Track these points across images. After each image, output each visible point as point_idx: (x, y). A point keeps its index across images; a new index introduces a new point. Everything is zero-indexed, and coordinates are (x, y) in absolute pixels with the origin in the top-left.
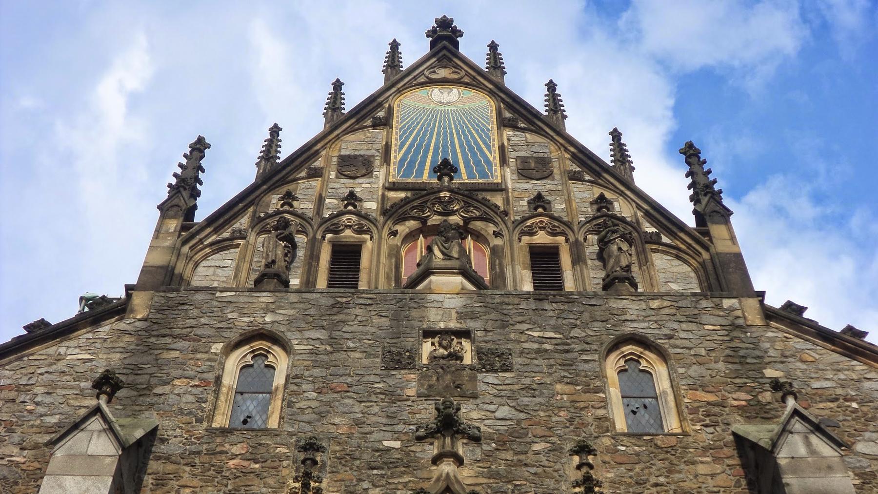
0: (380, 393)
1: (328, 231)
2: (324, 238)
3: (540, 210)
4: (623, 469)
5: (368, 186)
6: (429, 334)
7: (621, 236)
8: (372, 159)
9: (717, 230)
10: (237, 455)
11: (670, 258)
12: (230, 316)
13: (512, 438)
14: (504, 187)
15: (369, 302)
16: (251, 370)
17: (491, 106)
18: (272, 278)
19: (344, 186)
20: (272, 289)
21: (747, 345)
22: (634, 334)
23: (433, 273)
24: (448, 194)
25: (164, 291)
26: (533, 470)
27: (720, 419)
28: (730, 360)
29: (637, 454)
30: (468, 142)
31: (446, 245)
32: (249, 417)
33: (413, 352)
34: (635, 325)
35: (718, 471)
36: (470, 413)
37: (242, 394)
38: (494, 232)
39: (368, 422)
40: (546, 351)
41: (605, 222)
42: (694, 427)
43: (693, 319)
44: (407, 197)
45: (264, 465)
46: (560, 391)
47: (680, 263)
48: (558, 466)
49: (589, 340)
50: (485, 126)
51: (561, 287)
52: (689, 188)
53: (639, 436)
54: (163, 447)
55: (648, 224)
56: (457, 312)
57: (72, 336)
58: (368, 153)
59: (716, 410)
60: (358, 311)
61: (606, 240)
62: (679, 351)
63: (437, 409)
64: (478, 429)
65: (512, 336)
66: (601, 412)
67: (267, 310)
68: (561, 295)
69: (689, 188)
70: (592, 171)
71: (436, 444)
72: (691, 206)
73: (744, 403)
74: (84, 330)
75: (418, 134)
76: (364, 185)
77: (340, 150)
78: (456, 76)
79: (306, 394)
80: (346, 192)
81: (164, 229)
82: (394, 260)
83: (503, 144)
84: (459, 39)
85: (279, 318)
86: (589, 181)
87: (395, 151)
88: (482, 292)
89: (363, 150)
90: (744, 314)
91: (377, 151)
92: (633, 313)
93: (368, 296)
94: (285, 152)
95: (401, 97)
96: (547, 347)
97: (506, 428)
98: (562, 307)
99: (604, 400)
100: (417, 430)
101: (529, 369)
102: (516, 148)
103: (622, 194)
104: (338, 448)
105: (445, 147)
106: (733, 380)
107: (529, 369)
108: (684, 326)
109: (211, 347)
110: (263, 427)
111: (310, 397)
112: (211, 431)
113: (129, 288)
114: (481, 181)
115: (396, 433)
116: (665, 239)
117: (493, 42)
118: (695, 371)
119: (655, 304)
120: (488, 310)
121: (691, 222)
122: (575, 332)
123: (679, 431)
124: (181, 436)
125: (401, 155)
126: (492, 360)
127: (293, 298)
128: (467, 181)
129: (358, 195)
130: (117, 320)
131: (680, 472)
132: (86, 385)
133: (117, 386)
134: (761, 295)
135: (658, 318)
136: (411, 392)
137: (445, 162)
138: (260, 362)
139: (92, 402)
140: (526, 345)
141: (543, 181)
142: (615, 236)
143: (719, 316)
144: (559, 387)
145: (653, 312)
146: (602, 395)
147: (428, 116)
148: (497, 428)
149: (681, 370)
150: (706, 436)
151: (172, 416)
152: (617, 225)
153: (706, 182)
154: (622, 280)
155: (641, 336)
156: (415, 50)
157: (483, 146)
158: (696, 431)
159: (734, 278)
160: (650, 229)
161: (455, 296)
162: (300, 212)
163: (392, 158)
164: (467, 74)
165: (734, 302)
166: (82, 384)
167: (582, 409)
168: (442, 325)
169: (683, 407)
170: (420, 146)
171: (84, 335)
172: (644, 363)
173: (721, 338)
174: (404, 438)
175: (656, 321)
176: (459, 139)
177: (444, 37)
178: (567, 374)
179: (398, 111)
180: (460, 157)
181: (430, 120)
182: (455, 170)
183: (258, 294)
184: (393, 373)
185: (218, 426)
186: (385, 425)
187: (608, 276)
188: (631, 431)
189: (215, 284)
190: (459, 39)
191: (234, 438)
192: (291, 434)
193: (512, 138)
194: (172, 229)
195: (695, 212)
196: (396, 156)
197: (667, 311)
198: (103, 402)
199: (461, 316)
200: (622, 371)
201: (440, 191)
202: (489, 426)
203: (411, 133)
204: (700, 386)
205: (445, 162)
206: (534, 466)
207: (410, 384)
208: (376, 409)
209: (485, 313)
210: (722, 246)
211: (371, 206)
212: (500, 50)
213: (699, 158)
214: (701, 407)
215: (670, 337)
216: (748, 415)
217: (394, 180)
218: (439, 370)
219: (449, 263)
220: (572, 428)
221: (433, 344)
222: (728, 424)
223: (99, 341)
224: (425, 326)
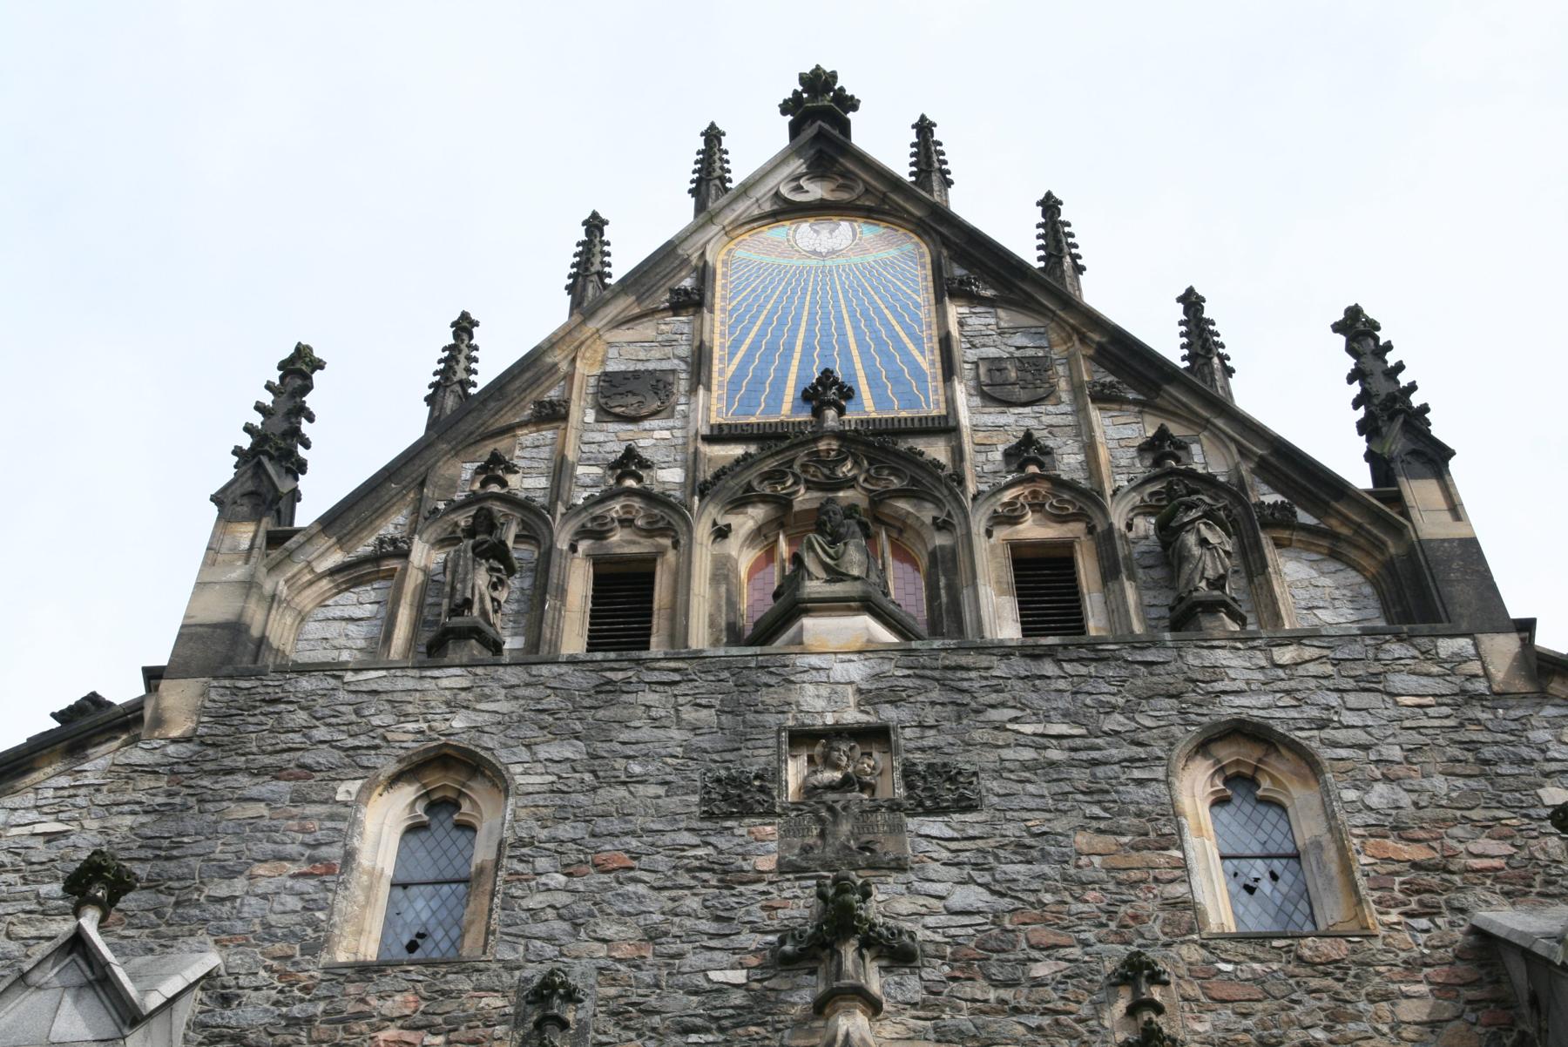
0: (702, 869)
1: (583, 533)
2: (573, 548)
3: (1033, 469)
4: (1227, 1013)
5: (666, 434)
6: (802, 738)
7: (1206, 515)
8: (671, 378)
9: (1420, 493)
10: (392, 1020)
11: (1316, 557)
12: (376, 721)
13: (981, 956)
14: (952, 423)
15: (677, 677)
16: (423, 835)
17: (922, 256)
18: (448, 634)
19: (614, 439)
20: (465, 660)
21: (1500, 737)
22: (1242, 722)
23: (807, 612)
24: (835, 445)
25: (231, 677)
26: (1034, 1021)
27: (1441, 899)
28: (1459, 768)
29: (1257, 980)
30: (874, 331)
31: (831, 551)
32: (421, 936)
33: (769, 775)
34: (1238, 701)
35: (1446, 1015)
36: (887, 902)
37: (405, 886)
38: (935, 519)
39: (675, 930)
40: (1052, 764)
41: (1172, 487)
42: (1386, 918)
43: (1371, 684)
44: (747, 455)
45: (452, 1036)
46: (1085, 848)
47: (1339, 566)
48: (1085, 1010)
49: (1142, 736)
50: (910, 298)
51: (1081, 629)
52: (1356, 404)
53: (1262, 938)
54: (228, 1013)
55: (1264, 488)
56: (859, 691)
57: (20, 784)
58: (666, 365)
59: (1433, 879)
60: (650, 698)
61: (1173, 524)
62: (1343, 753)
63: (821, 895)
64: (912, 935)
65: (977, 735)
66: (1178, 890)
67: (453, 706)
68: (1080, 646)
69: (1356, 404)
70: (1139, 381)
71: (821, 972)
72: (1361, 444)
73: (1496, 863)
74: (49, 770)
75: (767, 322)
76: (657, 434)
77: (603, 362)
78: (844, 196)
79: (543, 879)
80: (620, 449)
81: (228, 542)
82: (723, 589)
83: (948, 334)
84: (851, 115)
85: (480, 719)
86: (1135, 402)
87: (721, 359)
88: (914, 644)
89: (654, 362)
90: (1485, 669)
91: (682, 359)
92: (1238, 675)
93: (672, 665)
94: (486, 373)
95: (731, 246)
96: (1055, 754)
97: (971, 931)
98: (1083, 670)
99: (1183, 865)
100: (782, 942)
101: (1015, 803)
102: (976, 341)
103: (1205, 425)
104: (612, 991)
105: (826, 345)
106: (1466, 813)
107: (1015, 803)
108: (1352, 700)
109: (335, 791)
110: (451, 954)
111: (552, 884)
112: (336, 973)
113: (153, 676)
114: (903, 414)
115: (734, 951)
116: (1304, 517)
117: (923, 118)
118: (1379, 795)
119: (1285, 655)
120: (926, 683)
121: (1360, 477)
122: (1115, 722)
123: (1353, 926)
124: (270, 987)
125: (733, 367)
126: (941, 789)
127: (511, 675)
128: (874, 415)
129: (645, 455)
130: (126, 744)
131: (1357, 1018)
132: (56, 888)
133: (121, 885)
134: (1526, 627)
135: (1293, 684)
136: (766, 863)
137: (827, 376)
138: (443, 816)
139: (62, 928)
140: (1008, 754)
141: (1036, 408)
142: (1193, 514)
143: (1428, 675)
144: (1082, 840)
145: (1281, 673)
146: (1177, 854)
147: (789, 283)
148: (952, 931)
149: (1350, 795)
150: (1415, 938)
151: (248, 944)
152: (1197, 492)
153: (1392, 389)
154: (1212, 607)
155: (1258, 725)
156: (759, 141)
157: (906, 340)
158: (1390, 926)
159: (1460, 593)
160: (1272, 498)
161: (855, 657)
162: (522, 495)
163: (715, 375)
164: (868, 191)
165: (1464, 644)
166: (44, 889)
167: (1133, 885)
168: (830, 720)
169: (1358, 875)
170: (772, 348)
171: (50, 778)
172: (1266, 783)
173: (1437, 723)
174: (754, 961)
175: (1288, 692)
176: (856, 328)
177: (819, 110)
178: (1097, 810)
179: (724, 275)
180: (858, 366)
181: (794, 292)
182: (847, 393)
183: (436, 673)
184: (729, 824)
185: (750, 510)
186: (712, 936)
187: (1180, 599)
188: (1243, 929)
189: (345, 656)
190: (851, 115)
191: (387, 983)
192: (510, 967)
193: (970, 321)
194: (245, 544)
195: (1370, 456)
196: (722, 369)
197: (1313, 668)
198: (89, 922)
199: (866, 698)
200: (1220, 802)
201: (816, 440)
202: (934, 929)
203: (753, 321)
204: (1394, 828)
205: (827, 376)
206: (1033, 1012)
207: (763, 844)
208: (693, 903)
209: (919, 690)
210: (1430, 522)
211: (670, 477)
212: (938, 135)
213: (1377, 339)
214: (1398, 874)
215: (1323, 725)
216: (1507, 888)
217: (721, 420)
218: (824, 813)
219: (839, 589)
220: (1113, 925)
221: (811, 760)
222: (1462, 911)
223: (82, 791)
224: (791, 723)
